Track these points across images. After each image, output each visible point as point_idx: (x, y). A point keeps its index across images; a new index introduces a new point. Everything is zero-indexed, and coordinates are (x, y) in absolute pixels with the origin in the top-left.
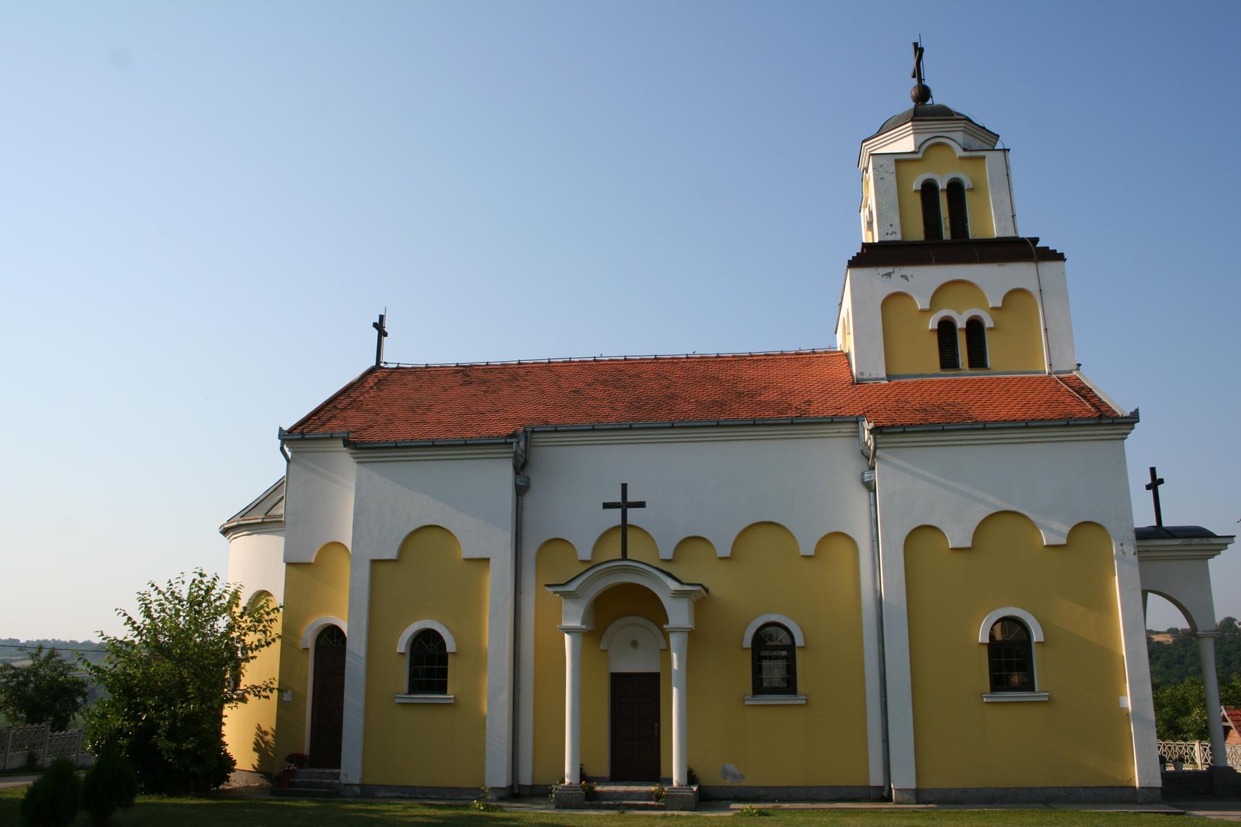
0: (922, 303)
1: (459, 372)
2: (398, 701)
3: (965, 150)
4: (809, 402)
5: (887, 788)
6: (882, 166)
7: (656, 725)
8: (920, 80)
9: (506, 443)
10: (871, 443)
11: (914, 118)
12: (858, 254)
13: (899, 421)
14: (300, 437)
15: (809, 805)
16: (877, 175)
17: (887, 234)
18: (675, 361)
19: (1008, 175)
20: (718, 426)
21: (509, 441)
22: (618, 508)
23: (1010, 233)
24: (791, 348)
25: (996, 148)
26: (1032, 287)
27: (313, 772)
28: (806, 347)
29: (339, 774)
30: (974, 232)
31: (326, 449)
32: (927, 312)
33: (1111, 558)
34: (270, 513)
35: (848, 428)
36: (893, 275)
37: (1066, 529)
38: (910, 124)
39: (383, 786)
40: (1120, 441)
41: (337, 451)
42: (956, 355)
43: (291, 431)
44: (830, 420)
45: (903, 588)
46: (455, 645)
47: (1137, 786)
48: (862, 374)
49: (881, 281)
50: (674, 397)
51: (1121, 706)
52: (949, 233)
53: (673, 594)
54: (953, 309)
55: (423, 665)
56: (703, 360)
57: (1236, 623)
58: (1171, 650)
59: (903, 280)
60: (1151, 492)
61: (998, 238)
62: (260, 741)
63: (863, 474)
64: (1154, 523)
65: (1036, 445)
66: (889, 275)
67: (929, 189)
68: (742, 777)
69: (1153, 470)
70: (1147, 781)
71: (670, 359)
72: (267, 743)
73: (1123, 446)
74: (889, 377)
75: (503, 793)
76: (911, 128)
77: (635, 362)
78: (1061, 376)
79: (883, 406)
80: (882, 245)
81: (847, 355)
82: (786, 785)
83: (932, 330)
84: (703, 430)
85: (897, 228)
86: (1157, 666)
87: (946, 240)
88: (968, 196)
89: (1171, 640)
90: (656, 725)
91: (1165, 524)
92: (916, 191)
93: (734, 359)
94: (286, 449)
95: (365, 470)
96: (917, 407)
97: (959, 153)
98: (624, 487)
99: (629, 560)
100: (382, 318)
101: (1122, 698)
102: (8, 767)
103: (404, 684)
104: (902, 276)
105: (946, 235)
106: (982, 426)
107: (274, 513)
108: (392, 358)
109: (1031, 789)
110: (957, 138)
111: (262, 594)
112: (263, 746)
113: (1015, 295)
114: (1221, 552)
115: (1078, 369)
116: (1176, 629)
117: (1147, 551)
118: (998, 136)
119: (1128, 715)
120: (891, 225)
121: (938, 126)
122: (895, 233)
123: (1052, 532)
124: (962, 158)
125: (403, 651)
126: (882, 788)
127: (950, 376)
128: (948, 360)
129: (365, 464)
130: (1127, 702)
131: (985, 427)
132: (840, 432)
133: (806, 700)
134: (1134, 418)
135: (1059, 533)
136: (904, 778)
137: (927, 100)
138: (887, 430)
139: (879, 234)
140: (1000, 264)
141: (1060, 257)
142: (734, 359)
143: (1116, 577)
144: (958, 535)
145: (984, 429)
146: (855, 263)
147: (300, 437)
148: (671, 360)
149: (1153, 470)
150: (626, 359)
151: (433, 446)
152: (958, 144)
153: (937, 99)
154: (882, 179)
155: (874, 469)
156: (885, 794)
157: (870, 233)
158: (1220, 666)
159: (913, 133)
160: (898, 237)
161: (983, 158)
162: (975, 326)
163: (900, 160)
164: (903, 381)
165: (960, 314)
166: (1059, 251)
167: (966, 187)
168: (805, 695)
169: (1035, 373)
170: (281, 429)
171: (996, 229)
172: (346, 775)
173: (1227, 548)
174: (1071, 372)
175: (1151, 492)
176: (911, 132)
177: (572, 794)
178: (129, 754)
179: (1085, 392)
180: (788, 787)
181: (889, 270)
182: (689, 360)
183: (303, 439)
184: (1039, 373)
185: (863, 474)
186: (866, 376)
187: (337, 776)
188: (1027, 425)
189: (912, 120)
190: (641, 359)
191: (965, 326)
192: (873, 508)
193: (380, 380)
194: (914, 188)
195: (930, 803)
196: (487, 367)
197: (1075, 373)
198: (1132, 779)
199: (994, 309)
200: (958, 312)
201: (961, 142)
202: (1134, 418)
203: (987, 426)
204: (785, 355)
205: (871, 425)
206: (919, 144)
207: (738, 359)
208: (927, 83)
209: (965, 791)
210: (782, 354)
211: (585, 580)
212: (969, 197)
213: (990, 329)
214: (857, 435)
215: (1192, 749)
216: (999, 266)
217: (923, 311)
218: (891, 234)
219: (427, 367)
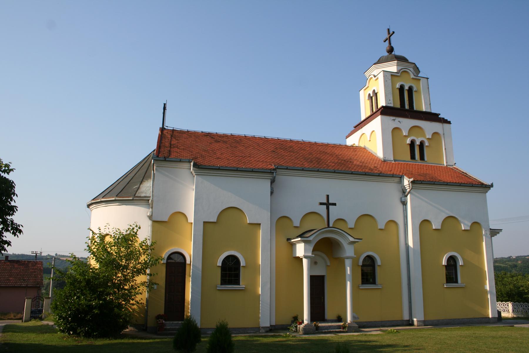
5: (411, 321)
6: (386, 76)
7: (322, 297)
8: (390, 43)
9: (271, 172)
14: (164, 159)
17: (388, 103)
19: (428, 88)
21: (272, 171)
22: (325, 205)
23: (429, 110)
25: (419, 76)
27: (173, 323)
31: (174, 167)
33: (482, 236)
34: (136, 195)
35: (397, 180)
36: (395, 120)
37: (470, 224)
38: (396, 61)
39: (210, 328)
40: (485, 194)
41: (180, 168)
45: (419, 243)
46: (244, 262)
47: (490, 316)
48: (385, 158)
51: (485, 288)
52: (408, 106)
53: (349, 243)
54: (416, 137)
55: (234, 273)
56: (285, 141)
59: (399, 123)
63: (401, 198)
65: (463, 192)
66: (394, 120)
67: (402, 88)
68: (358, 318)
70: (494, 315)
73: (486, 195)
74: (395, 160)
75: (268, 329)
76: (396, 63)
82: (374, 320)
83: (408, 144)
84: (326, 173)
85: (392, 101)
87: (407, 109)
90: (322, 297)
95: (200, 178)
98: (328, 196)
99: (331, 227)
101: (485, 286)
104: (399, 121)
105: (407, 107)
106: (446, 184)
109: (459, 319)
111: (3, 234)
113: (435, 134)
114: (497, 235)
115: (455, 165)
118: (420, 72)
119: (487, 292)
120: (390, 100)
124: (413, 78)
126: (409, 320)
127: (413, 162)
128: (413, 157)
129: (200, 176)
130: (488, 287)
132: (394, 181)
134: (492, 186)
135: (468, 225)
140: (431, 122)
141: (449, 123)
143: (484, 243)
144: (436, 225)
145: (447, 185)
147: (164, 159)
151: (237, 170)
154: (386, 81)
156: (411, 323)
160: (392, 105)
163: (393, 75)
166: (448, 120)
169: (441, 165)
174: (453, 166)
176: (396, 64)
177: (311, 328)
180: (375, 321)
181: (394, 118)
183: (165, 160)
195: (428, 326)
196: (216, 135)
197: (454, 166)
198: (488, 315)
199: (428, 139)
203: (435, 183)
204: (329, 144)
209: (438, 321)
211: (316, 236)
213: (427, 146)
216: (431, 122)
217: (405, 136)
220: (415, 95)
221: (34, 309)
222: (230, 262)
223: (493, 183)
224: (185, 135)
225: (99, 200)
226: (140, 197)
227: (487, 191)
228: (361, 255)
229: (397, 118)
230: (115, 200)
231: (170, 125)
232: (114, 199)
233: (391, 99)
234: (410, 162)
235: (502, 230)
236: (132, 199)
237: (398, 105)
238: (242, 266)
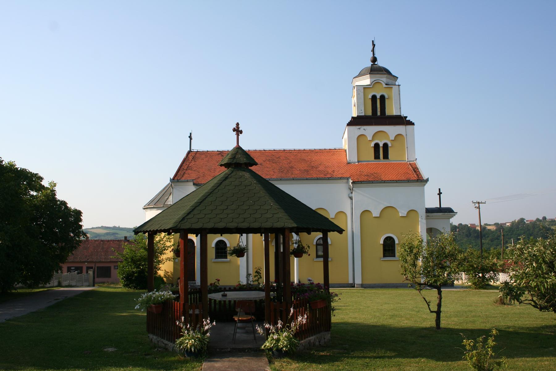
0: (370, 138)
1: (219, 154)
2: (213, 261)
3: (386, 84)
4: (334, 171)
5: (354, 284)
6: (359, 90)
8: (374, 54)
10: (351, 186)
11: (371, 73)
13: (360, 180)
14: (177, 181)
15: (332, 289)
18: (290, 151)
20: (307, 179)
23: (399, 114)
24: (328, 147)
26: (404, 134)
28: (332, 147)
29: (195, 283)
30: (388, 113)
34: (165, 204)
35: (345, 181)
37: (406, 213)
38: (369, 75)
42: (379, 155)
46: (398, 241)
48: (350, 160)
49: (358, 130)
50: (292, 167)
52: (380, 113)
57: (525, 221)
58: (494, 233)
60: (439, 195)
61: (395, 115)
62: (166, 275)
63: (349, 194)
66: (360, 128)
67: (374, 98)
69: (440, 189)
72: (169, 275)
74: (358, 162)
77: (277, 151)
78: (411, 162)
79: (356, 173)
80: (359, 117)
81: (346, 150)
85: (363, 111)
86: (487, 241)
88: (386, 100)
89: (495, 228)
91: (442, 206)
92: (370, 98)
93: (310, 151)
96: (366, 174)
97: (385, 86)
102: (54, 286)
103: (214, 257)
104: (364, 129)
105: (379, 114)
107: (167, 204)
109: (393, 284)
110: (383, 79)
112: (167, 276)
116: (498, 223)
118: (398, 78)
121: (378, 77)
123: (403, 213)
125: (214, 247)
126: (352, 284)
127: (377, 162)
128: (377, 157)
131: (384, 182)
133: (332, 259)
134: (427, 180)
136: (358, 281)
137: (376, 62)
139: (357, 113)
142: (310, 151)
144: (376, 213)
146: (349, 124)
147: (177, 181)
148: (289, 151)
149: (440, 189)
150: (274, 150)
152: (384, 82)
153: (380, 63)
154: (359, 94)
155: (352, 193)
156: (353, 285)
157: (355, 107)
158: (515, 241)
159: (370, 78)
160: (363, 114)
161: (392, 87)
162: (386, 146)
163: (365, 88)
164: (363, 163)
165: (381, 142)
167: (386, 98)
168: (331, 258)
171: (395, 113)
172: (198, 283)
173: (455, 216)
174: (414, 161)
175: (439, 195)
179: (416, 170)
181: (360, 127)
182: (295, 151)
183: (178, 181)
184: (404, 161)
185: (349, 194)
186: (351, 161)
187: (195, 283)
188: (397, 181)
189: (370, 74)
190: (279, 150)
191: (382, 146)
192: (352, 204)
193: (193, 157)
194: (369, 98)
197: (415, 162)
201: (385, 82)
202: (427, 180)
204: (326, 150)
205: (352, 181)
207: (311, 151)
208: (376, 56)
209: (375, 284)
210: (325, 150)
212: (387, 101)
213: (390, 147)
214: (348, 182)
215: (462, 275)
220: (387, 102)
222: (223, 245)
223: (428, 178)
224: (203, 156)
225: (146, 207)
226: (167, 205)
227: (425, 185)
228: (315, 238)
230: (154, 207)
231: (196, 147)
232: (153, 206)
233: (363, 109)
234: (373, 161)
235: (457, 212)
236: (162, 206)
237: (369, 113)
238: (396, 244)
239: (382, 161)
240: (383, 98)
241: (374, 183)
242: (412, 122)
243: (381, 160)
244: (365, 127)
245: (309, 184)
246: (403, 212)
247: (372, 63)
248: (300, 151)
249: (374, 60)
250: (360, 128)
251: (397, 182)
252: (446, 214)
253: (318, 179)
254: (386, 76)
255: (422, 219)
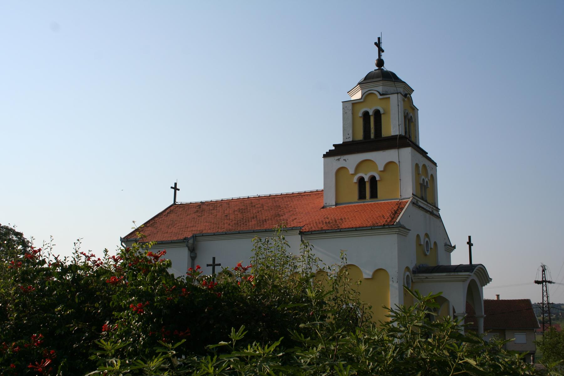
0: (352, 171)
9: (183, 242)
12: (327, 153)
16: (344, 111)
17: (346, 138)
21: (185, 241)
26: (397, 162)
32: (353, 175)
36: (340, 159)
37: (371, 274)
43: (124, 238)
44: (291, 229)
64: (468, 263)
66: (339, 160)
67: (366, 115)
69: (470, 237)
71: (275, 196)
74: (336, 205)
76: (359, 87)
84: (208, 237)
85: (351, 136)
91: (473, 263)
94: (123, 244)
97: (380, 97)
100: (176, 184)
104: (344, 160)
105: (372, 136)
108: (179, 201)
117: (433, 278)
122: (350, 138)
123: (367, 273)
124: (380, 99)
128: (362, 196)
138: (306, 233)
146: (325, 156)
149: (470, 237)
154: (346, 113)
159: (361, 89)
160: (351, 140)
161: (389, 98)
162: (373, 180)
163: (355, 103)
165: (366, 175)
170: (121, 237)
176: (360, 89)
178: (172, 340)
181: (339, 157)
200: (365, 174)
206: (362, 94)
208: (383, 58)
212: (383, 117)
213: (379, 180)
217: (352, 174)
218: (348, 138)
219: (191, 203)
221: (390, 344)
229: (342, 157)
233: (350, 132)
234: (359, 203)
239: (368, 202)
240: (377, 114)
241: (313, 234)
242: (327, 153)
243: (366, 200)
244: (346, 157)
245: (230, 240)
246: (368, 272)
247: (377, 68)
248: (288, 195)
249: (380, 63)
250: (339, 160)
251: (356, 230)
252: (453, 274)
253: (266, 231)
254: (381, 83)
255: (393, 281)
